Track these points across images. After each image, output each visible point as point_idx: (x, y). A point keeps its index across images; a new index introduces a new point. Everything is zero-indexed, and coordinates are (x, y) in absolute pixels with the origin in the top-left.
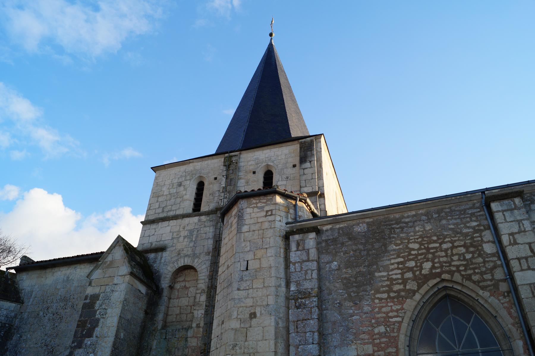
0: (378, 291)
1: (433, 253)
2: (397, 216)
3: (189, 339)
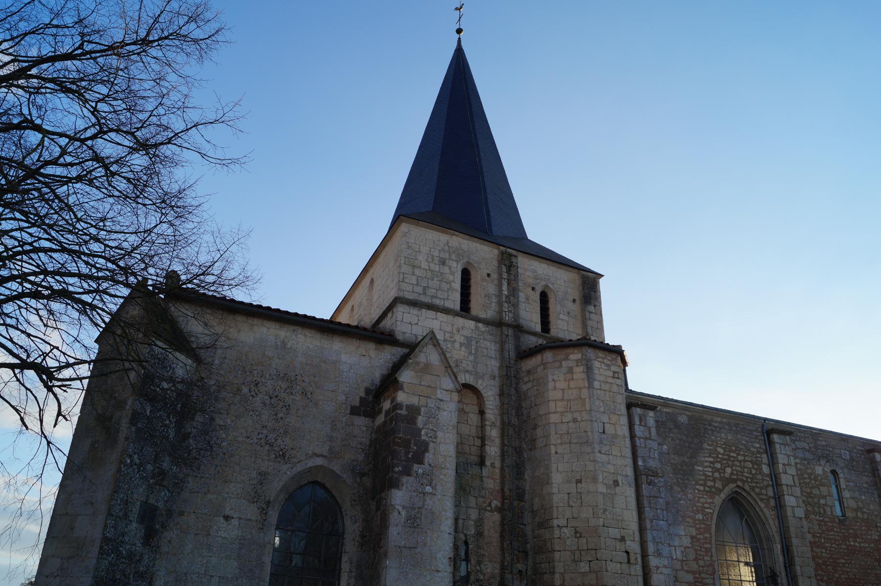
0: (697, 484)
1: (733, 461)
2: (709, 418)
3: (484, 479)
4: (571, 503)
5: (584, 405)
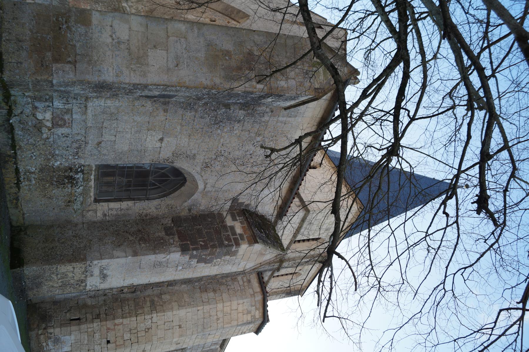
4: (166, 323)
5: (227, 323)
